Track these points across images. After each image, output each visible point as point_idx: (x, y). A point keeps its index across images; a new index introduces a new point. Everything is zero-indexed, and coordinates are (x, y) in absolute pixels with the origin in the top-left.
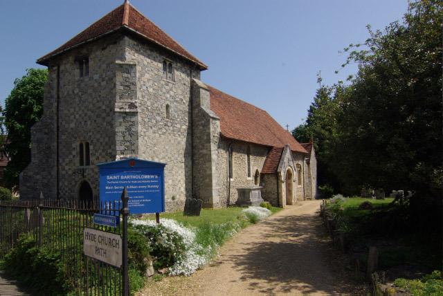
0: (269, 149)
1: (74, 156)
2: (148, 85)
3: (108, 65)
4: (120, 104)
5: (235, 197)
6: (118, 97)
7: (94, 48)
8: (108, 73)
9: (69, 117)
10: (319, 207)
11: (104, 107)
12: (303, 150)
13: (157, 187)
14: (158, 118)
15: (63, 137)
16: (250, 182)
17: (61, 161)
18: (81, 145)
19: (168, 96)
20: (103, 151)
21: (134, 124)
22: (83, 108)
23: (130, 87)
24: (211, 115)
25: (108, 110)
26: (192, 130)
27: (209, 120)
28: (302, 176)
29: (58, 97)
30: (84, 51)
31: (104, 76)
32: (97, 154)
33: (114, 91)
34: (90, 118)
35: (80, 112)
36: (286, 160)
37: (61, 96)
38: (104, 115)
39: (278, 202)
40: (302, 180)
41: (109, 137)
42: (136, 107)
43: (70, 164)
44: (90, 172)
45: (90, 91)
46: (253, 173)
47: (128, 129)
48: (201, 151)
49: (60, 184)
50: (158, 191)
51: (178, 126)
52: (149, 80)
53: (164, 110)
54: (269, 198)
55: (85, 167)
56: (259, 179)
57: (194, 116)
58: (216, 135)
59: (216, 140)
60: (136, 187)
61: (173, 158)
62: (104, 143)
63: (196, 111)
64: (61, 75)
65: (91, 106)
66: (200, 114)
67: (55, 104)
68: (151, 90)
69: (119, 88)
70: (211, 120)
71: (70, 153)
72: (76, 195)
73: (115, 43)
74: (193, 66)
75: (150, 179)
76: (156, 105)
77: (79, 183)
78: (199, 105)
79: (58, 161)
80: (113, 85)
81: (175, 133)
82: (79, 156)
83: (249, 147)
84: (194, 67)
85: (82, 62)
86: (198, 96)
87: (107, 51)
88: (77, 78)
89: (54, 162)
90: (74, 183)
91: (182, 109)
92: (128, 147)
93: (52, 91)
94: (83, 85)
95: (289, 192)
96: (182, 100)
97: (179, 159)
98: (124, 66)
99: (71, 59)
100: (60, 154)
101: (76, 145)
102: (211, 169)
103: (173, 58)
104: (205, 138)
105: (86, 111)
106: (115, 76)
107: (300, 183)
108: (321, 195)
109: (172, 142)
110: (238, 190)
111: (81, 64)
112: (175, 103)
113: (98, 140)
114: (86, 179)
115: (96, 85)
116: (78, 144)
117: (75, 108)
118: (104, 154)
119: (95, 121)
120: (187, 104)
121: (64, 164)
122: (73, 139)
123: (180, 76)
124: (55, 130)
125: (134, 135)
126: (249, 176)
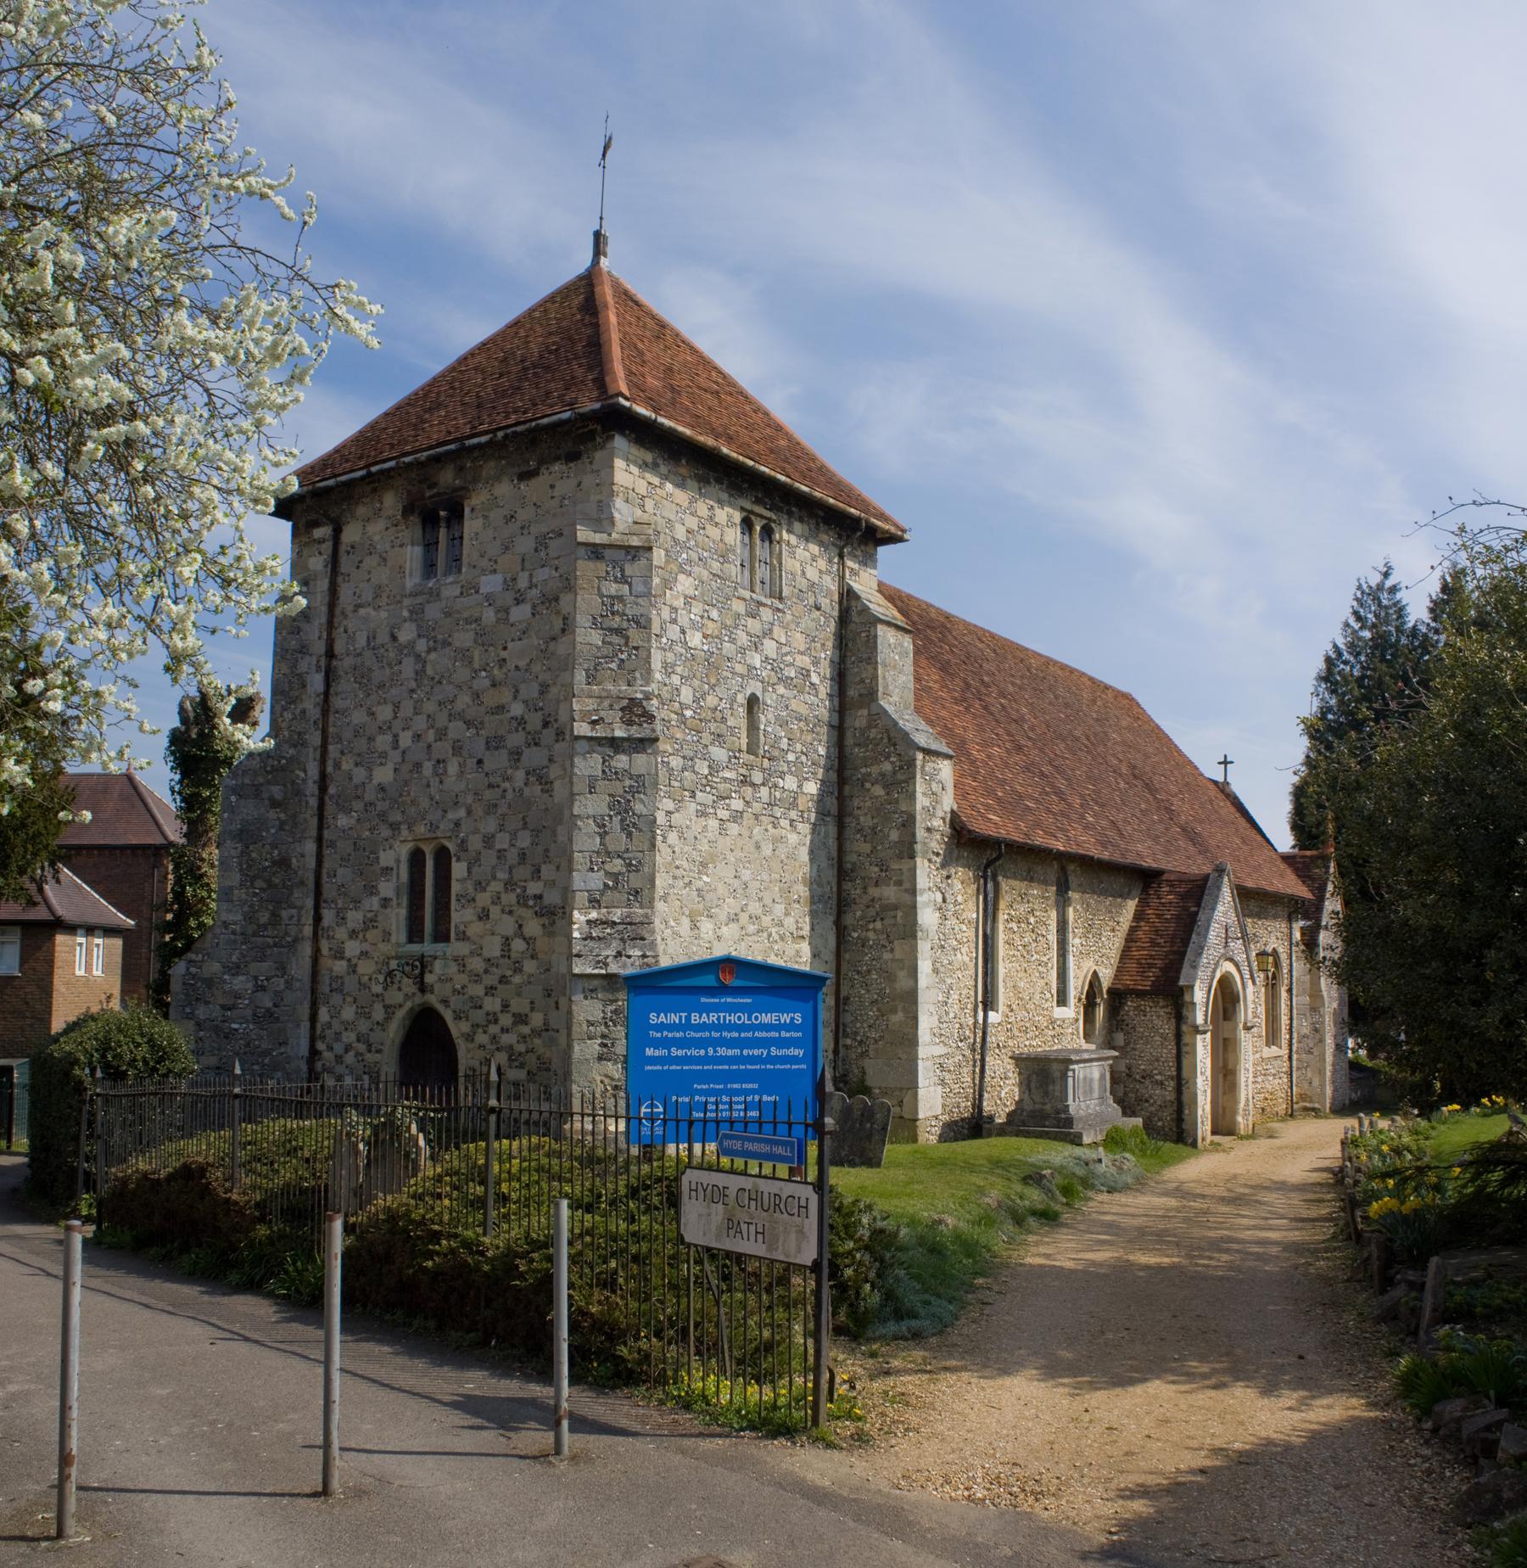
0: (1144, 879)
1: (385, 902)
2: (683, 619)
3: (542, 543)
4: (591, 704)
5: (1004, 1094)
6: (580, 676)
7: (490, 468)
8: (542, 574)
9: (371, 739)
10: (1335, 1151)
11: (517, 709)
12: (1303, 891)
13: (799, 1052)
14: (719, 754)
15: (343, 821)
16: (1064, 1027)
17: (328, 916)
18: (417, 858)
19: (757, 662)
20: (509, 885)
21: (641, 785)
22: (430, 707)
23: (628, 633)
24: (921, 739)
25: (535, 721)
26: (841, 799)
27: (911, 763)
28: (1284, 1009)
29: (330, 654)
30: (447, 477)
31: (523, 583)
32: (483, 899)
33: (561, 648)
34: (457, 748)
35: (420, 723)
36: (1214, 935)
37: (339, 648)
38: (516, 739)
39: (1179, 1118)
40: (1284, 1020)
41: (536, 832)
42: (650, 718)
43: (366, 938)
44: (453, 968)
45: (463, 638)
46: (1076, 986)
47: (621, 807)
48: (874, 892)
49: (324, 1015)
50: (804, 1066)
51: (790, 783)
52: (689, 600)
53: (739, 719)
54: (1141, 1100)
55: (427, 948)
56: (1100, 1012)
57: (849, 741)
58: (937, 823)
59: (936, 844)
60: (737, 1052)
61: (766, 921)
62: (512, 856)
63: (859, 719)
64: (345, 563)
65: (464, 700)
66: (873, 733)
67: (317, 682)
68: (695, 639)
69: (588, 637)
70: (920, 756)
71: (371, 890)
72: (389, 1065)
73: (573, 457)
74: (854, 530)
75: (779, 1027)
76: (711, 700)
77: (400, 1014)
78: (871, 695)
79: (318, 919)
80: (559, 624)
81: (778, 812)
82: (405, 902)
83: (1063, 869)
84: (854, 531)
85: (437, 515)
86: (871, 659)
87: (543, 479)
88: (411, 582)
89: (299, 923)
90: (378, 1013)
91: (803, 710)
92: (615, 876)
93: (305, 626)
94: (433, 612)
95: (1225, 1074)
96: (806, 674)
97: (789, 922)
98: (607, 553)
99: (391, 502)
100: (329, 891)
101: (396, 855)
102: (913, 972)
103: (780, 494)
104: (894, 835)
105: (442, 720)
106: (569, 584)
107: (1272, 1038)
108: (1363, 1092)
109: (767, 850)
110: (1019, 1060)
111: (430, 521)
112: (781, 690)
113: (488, 841)
114: (433, 999)
115: (489, 616)
116: (404, 851)
117: (397, 706)
118: (510, 898)
119: (480, 762)
120: (824, 691)
121: (341, 933)
122: (386, 832)
123: (804, 558)
124: (312, 788)
125: (642, 830)
126: (1062, 1000)
